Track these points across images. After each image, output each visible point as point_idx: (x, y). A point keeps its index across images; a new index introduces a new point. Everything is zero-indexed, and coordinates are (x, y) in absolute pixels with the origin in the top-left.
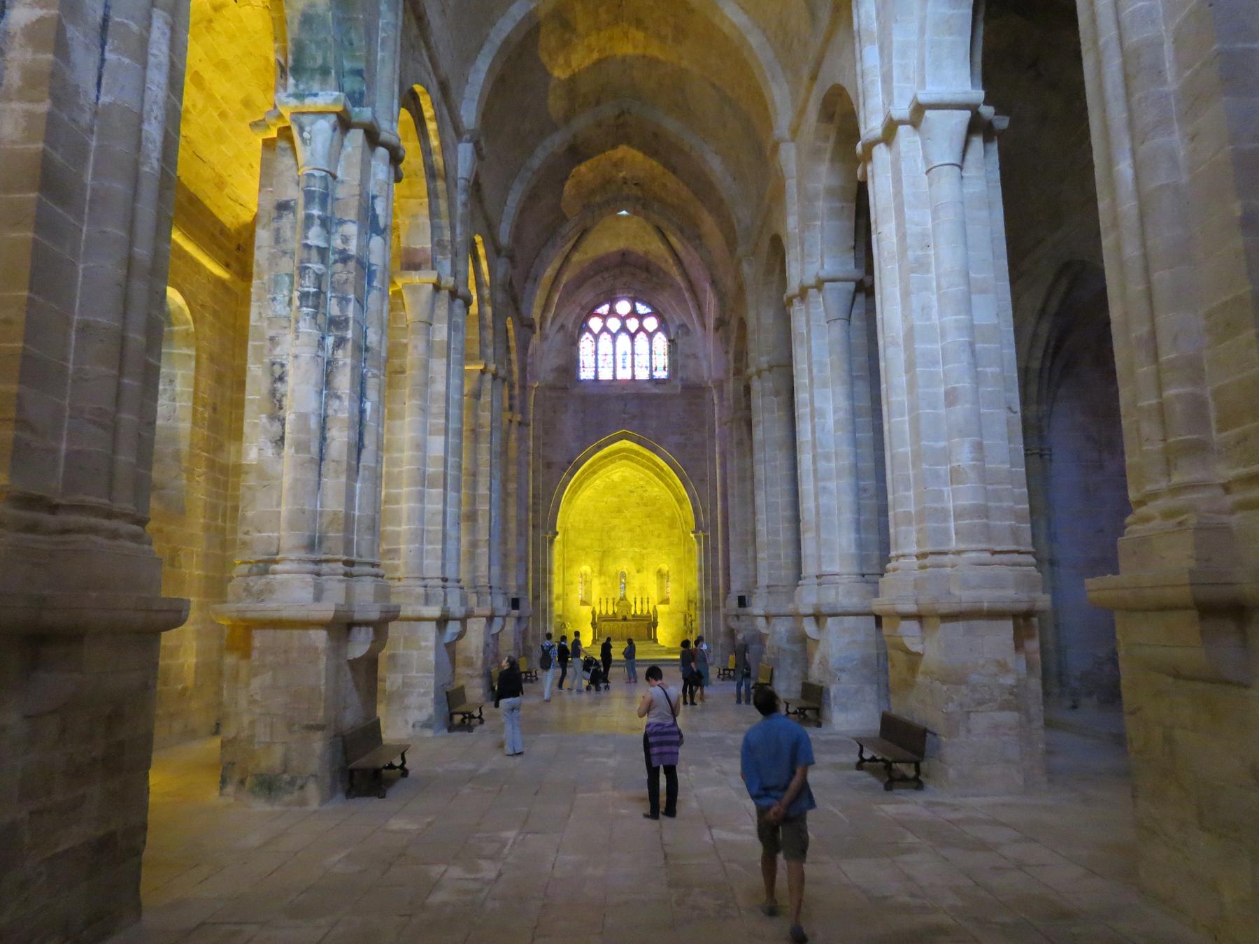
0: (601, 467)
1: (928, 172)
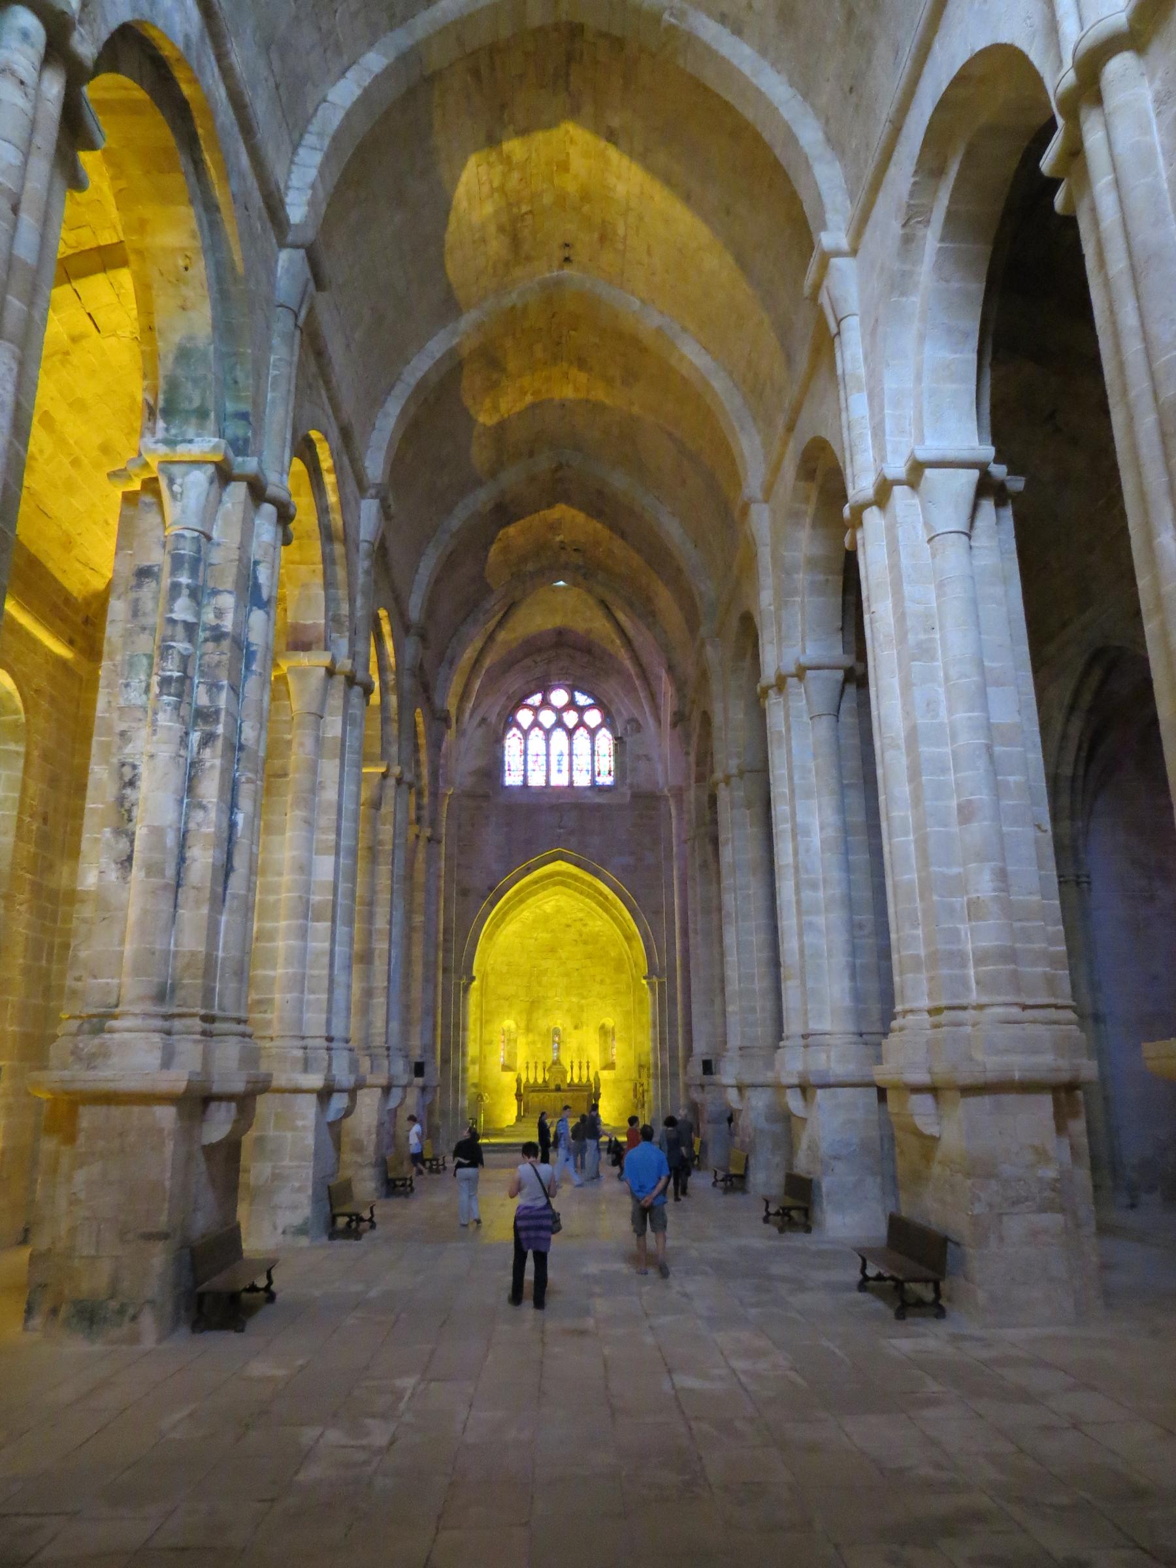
0: (531, 894)
1: (930, 541)
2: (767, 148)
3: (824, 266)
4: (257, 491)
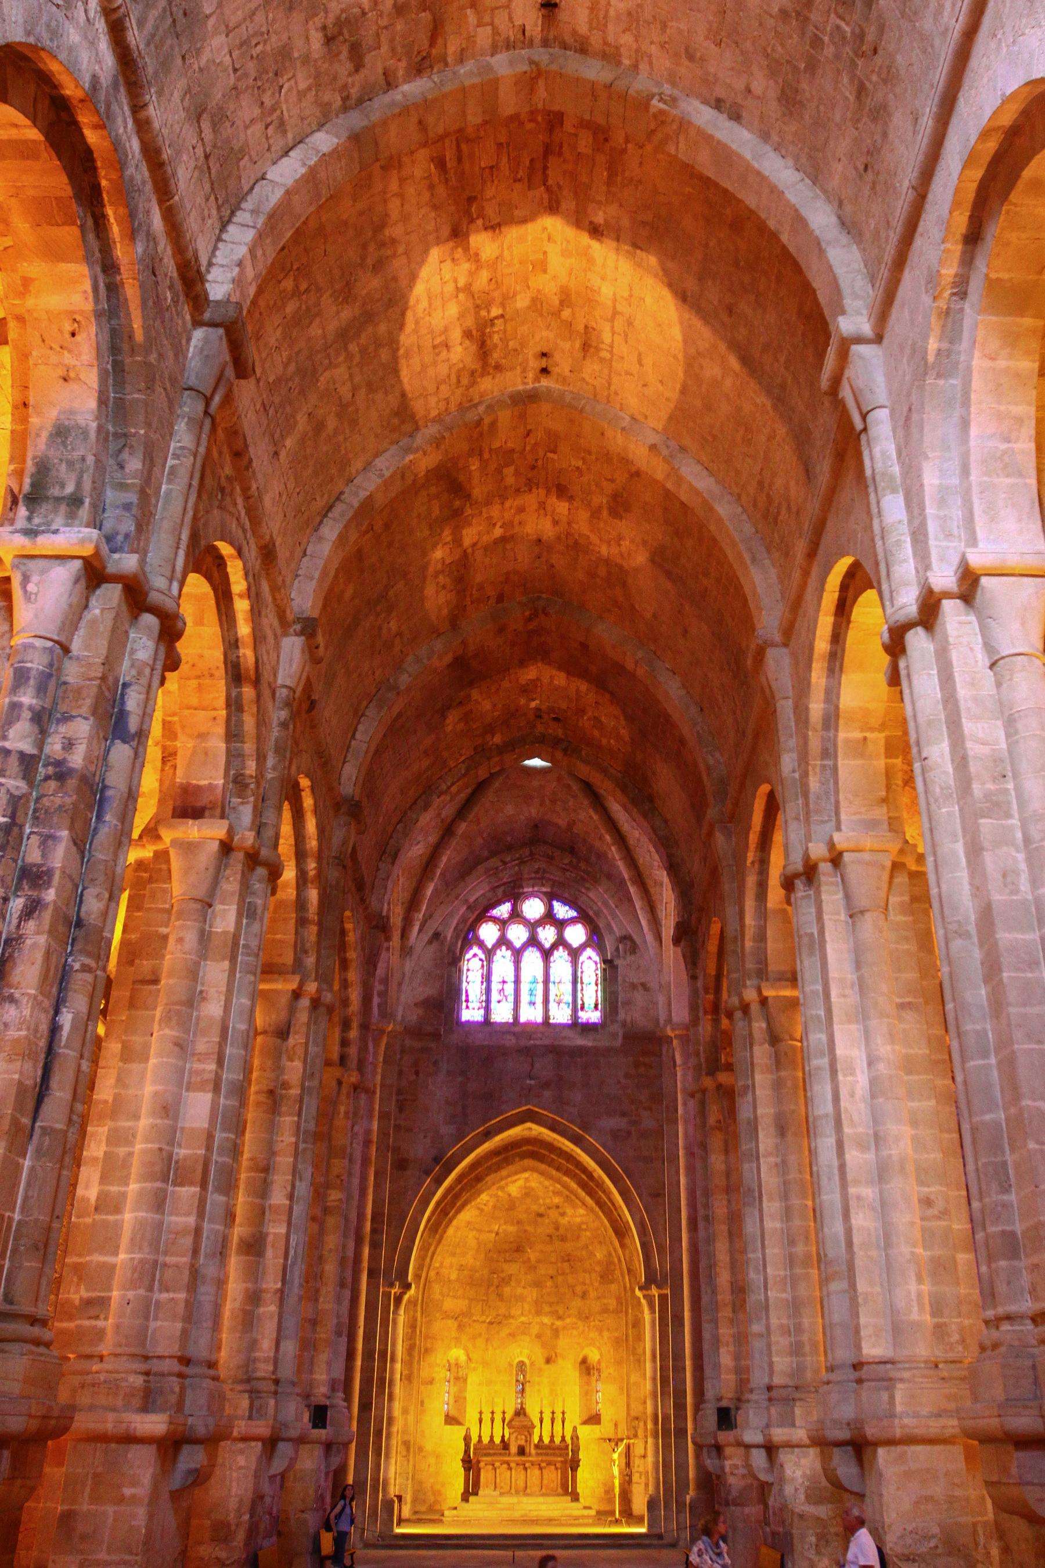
1: (992, 666)
2: (774, 237)
3: (844, 355)
4: (136, 596)
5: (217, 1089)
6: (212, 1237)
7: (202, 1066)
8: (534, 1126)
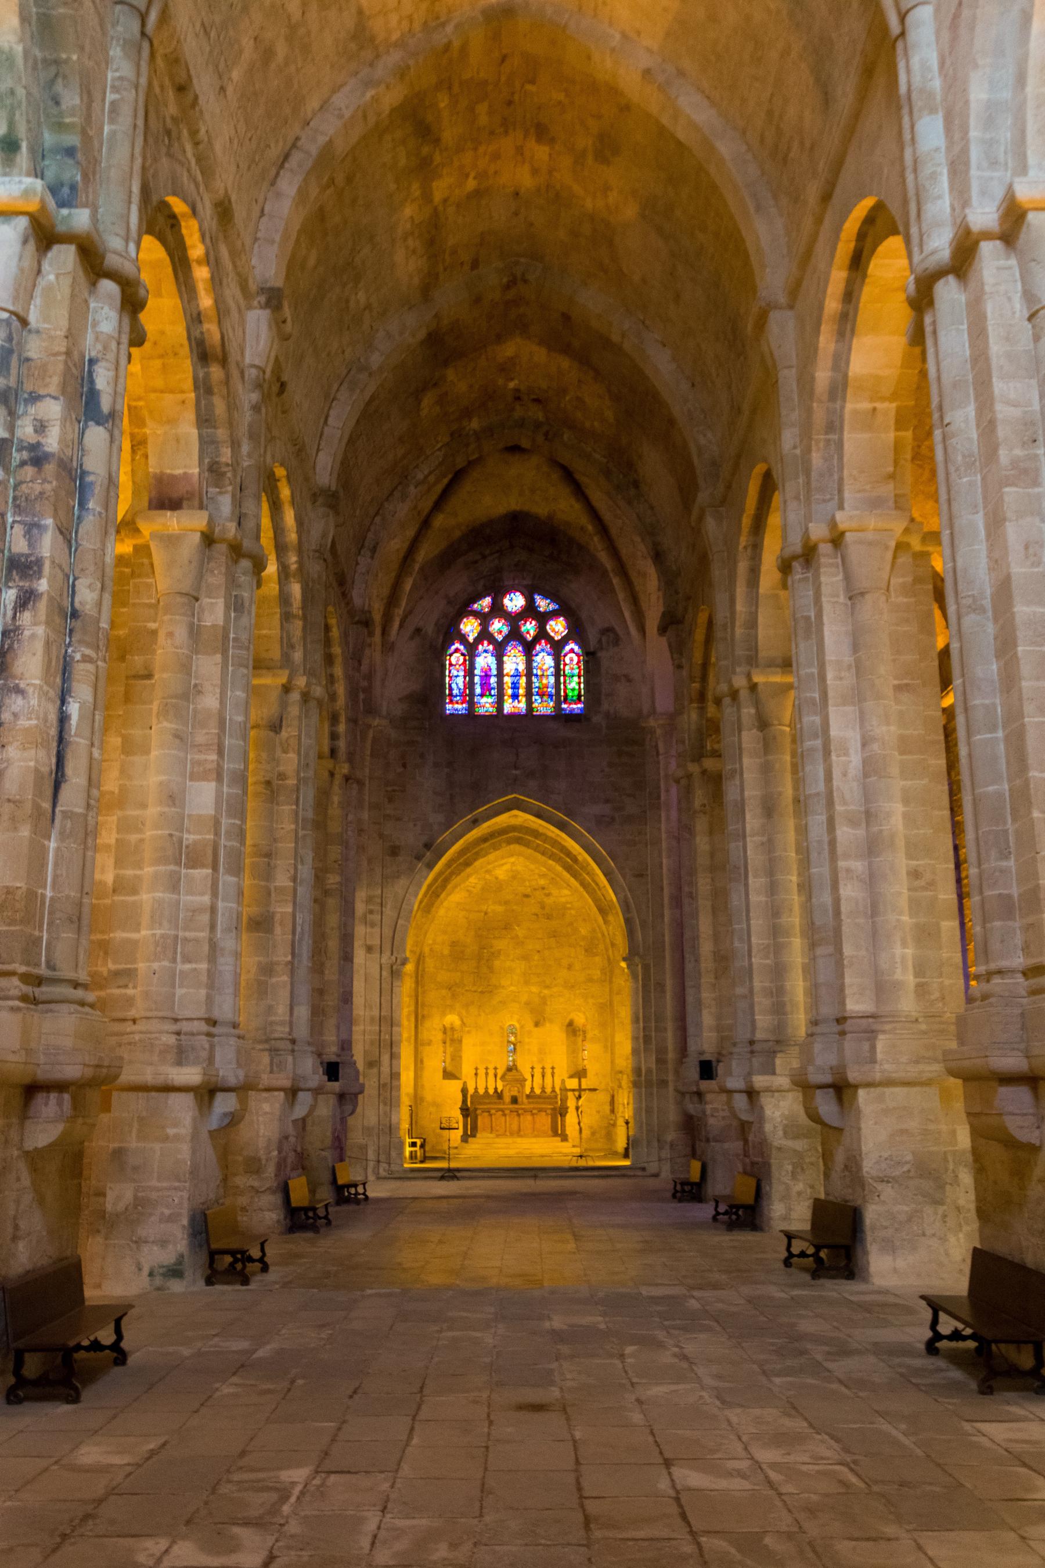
0: (477, 856)
1: (1030, 318)
4: (93, 261)
5: (219, 778)
6: (227, 914)
7: (202, 757)
8: (520, 813)
